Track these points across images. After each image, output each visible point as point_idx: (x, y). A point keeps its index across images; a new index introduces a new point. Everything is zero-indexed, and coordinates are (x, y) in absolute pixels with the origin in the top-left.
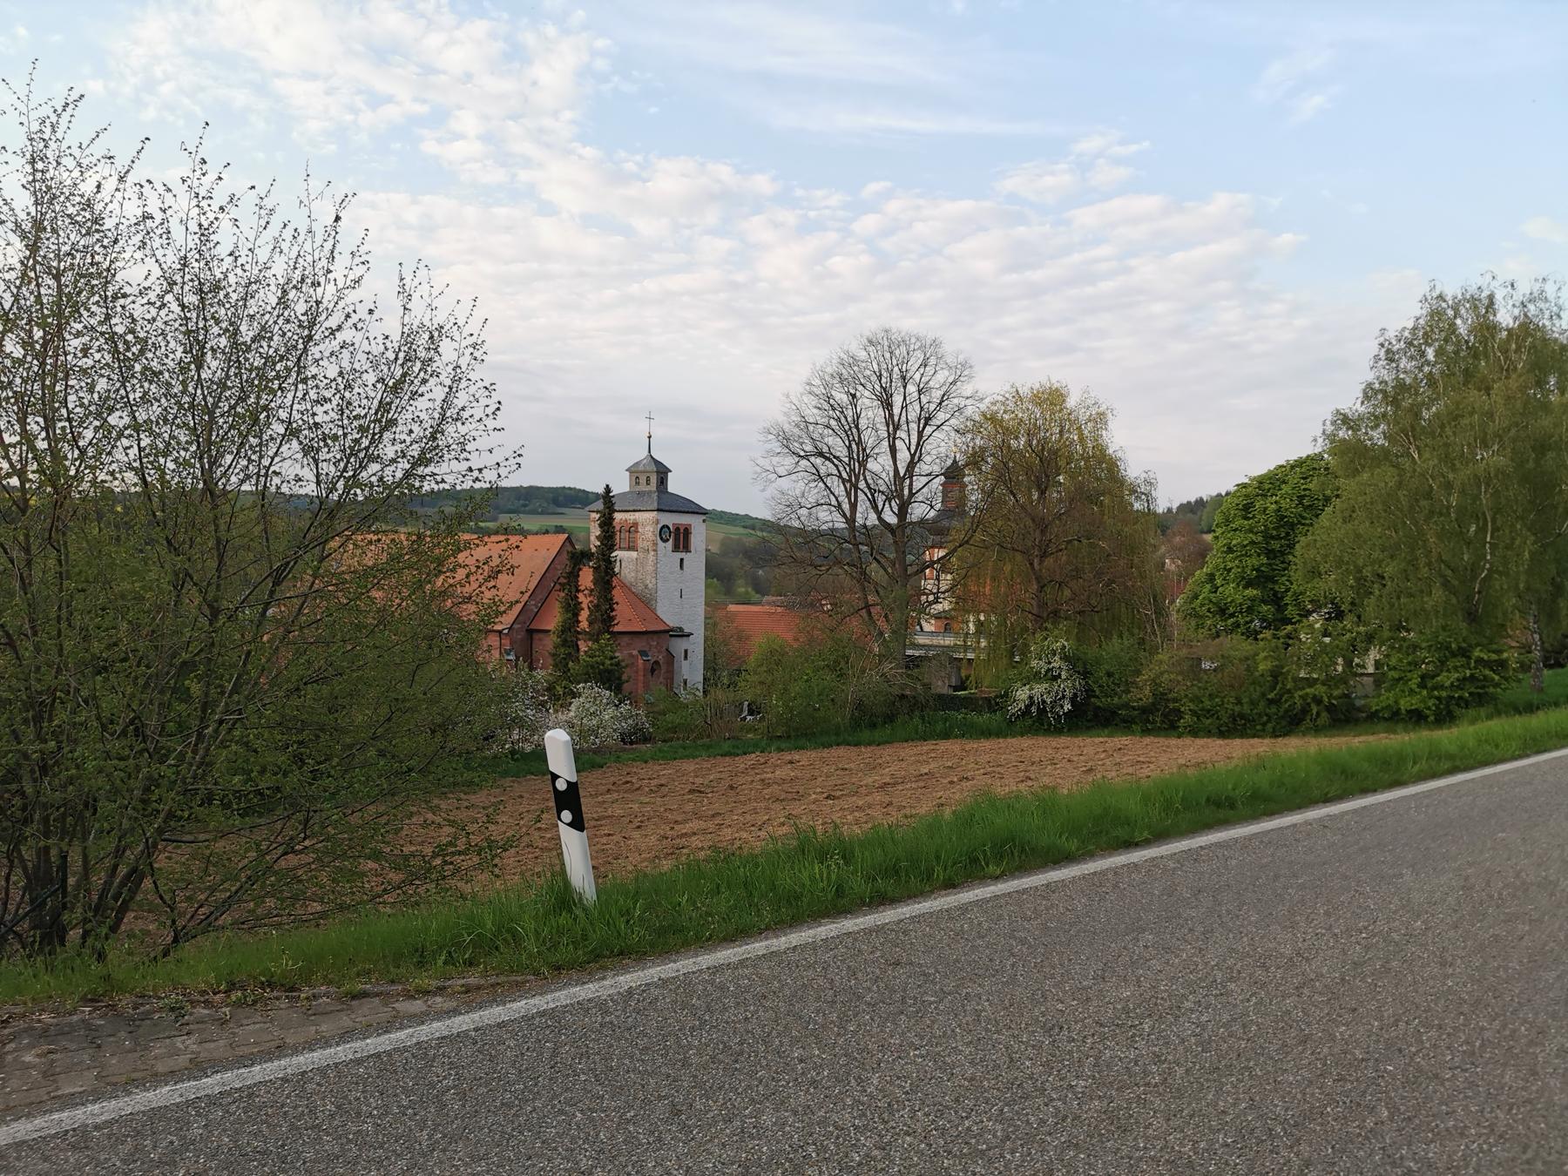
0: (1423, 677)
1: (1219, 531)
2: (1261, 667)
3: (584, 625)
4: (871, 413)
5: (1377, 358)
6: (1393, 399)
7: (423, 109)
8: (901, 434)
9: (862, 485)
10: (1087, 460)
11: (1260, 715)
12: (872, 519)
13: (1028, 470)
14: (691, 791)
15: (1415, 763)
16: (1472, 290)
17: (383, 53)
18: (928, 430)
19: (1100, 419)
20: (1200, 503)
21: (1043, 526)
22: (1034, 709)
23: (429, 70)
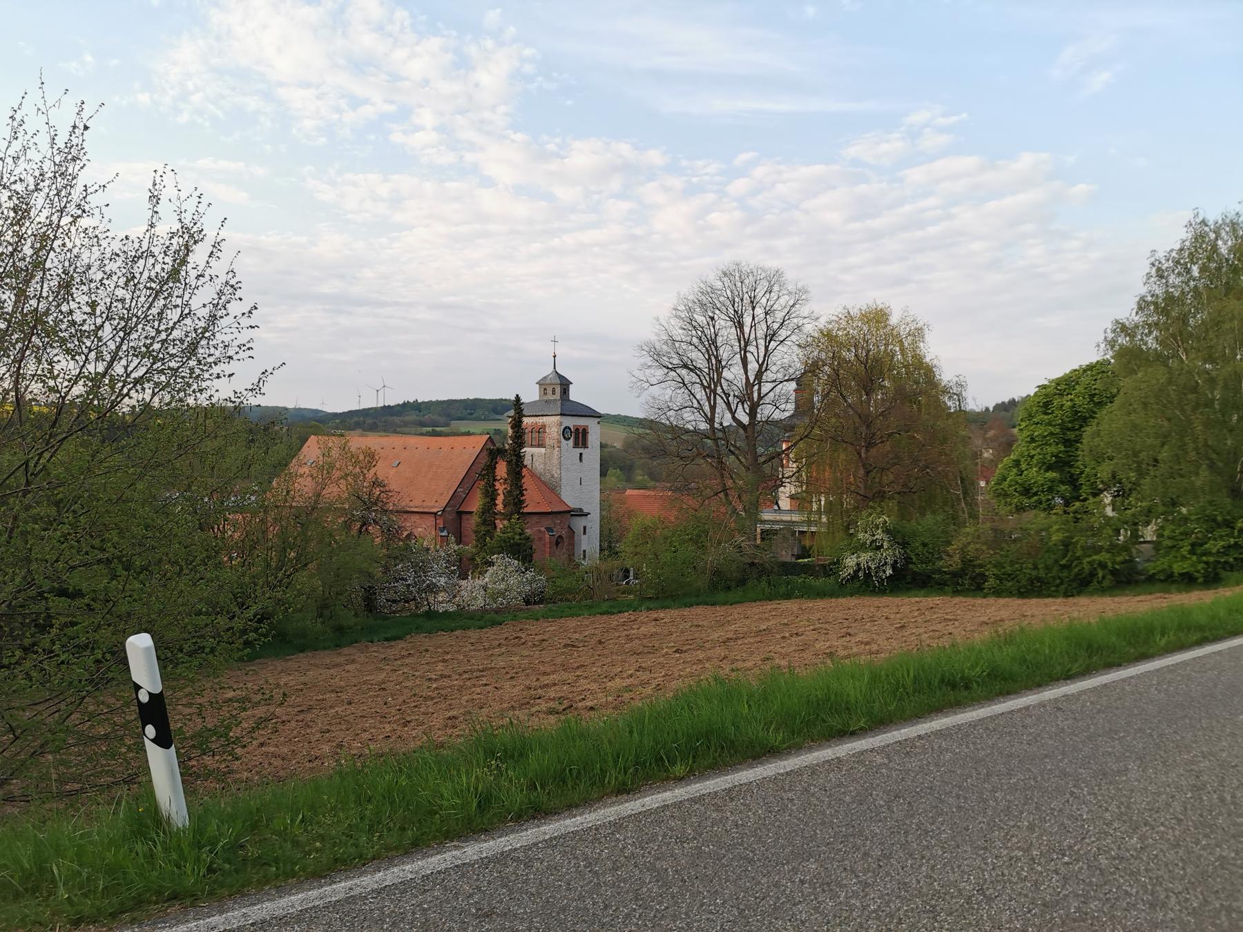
0: (1193, 545)
1: (1024, 424)
2: (1054, 538)
3: (500, 507)
4: (727, 332)
5: (1149, 276)
6: (1165, 310)
7: (391, 108)
8: (751, 348)
9: (719, 390)
10: (906, 367)
12: (728, 421)
13: (855, 376)
14: (566, 646)
15: (1163, 635)
16: (1231, 215)
17: (361, 66)
19: (918, 334)
20: (1013, 403)
21: (867, 421)
22: (861, 574)
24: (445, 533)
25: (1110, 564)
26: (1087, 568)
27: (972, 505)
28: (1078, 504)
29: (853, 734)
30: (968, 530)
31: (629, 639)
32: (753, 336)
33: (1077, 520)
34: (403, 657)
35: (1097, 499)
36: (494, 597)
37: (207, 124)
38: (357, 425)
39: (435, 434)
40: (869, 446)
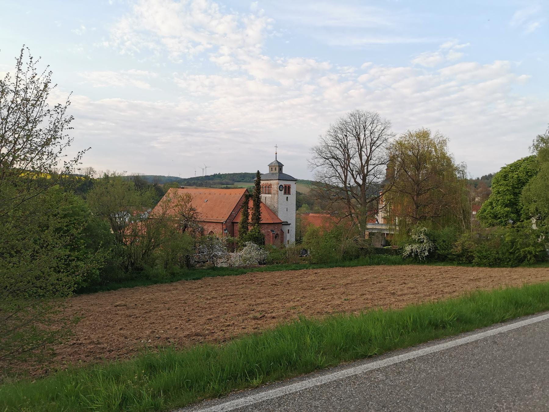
1: (495, 185)
3: (250, 221)
7: (209, 46)
8: (364, 149)
9: (349, 168)
10: (437, 158)
11: (506, 258)
12: (352, 183)
14: (272, 285)
17: (197, 28)
18: (374, 148)
20: (490, 176)
21: (418, 183)
22: (413, 254)
23: (212, 33)
24: (226, 232)
25: (533, 252)
26: (522, 254)
27: (468, 223)
28: (519, 223)
29: (370, 357)
30: (465, 235)
31: (302, 282)
32: (364, 144)
33: (518, 231)
34: (199, 288)
35: (528, 221)
36: (245, 260)
37: (133, 54)
38: (194, 184)
39: (227, 188)
40: (418, 195)
